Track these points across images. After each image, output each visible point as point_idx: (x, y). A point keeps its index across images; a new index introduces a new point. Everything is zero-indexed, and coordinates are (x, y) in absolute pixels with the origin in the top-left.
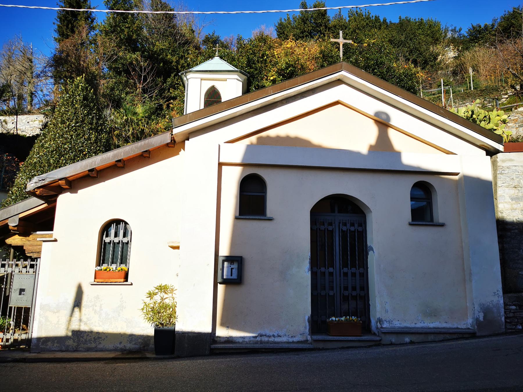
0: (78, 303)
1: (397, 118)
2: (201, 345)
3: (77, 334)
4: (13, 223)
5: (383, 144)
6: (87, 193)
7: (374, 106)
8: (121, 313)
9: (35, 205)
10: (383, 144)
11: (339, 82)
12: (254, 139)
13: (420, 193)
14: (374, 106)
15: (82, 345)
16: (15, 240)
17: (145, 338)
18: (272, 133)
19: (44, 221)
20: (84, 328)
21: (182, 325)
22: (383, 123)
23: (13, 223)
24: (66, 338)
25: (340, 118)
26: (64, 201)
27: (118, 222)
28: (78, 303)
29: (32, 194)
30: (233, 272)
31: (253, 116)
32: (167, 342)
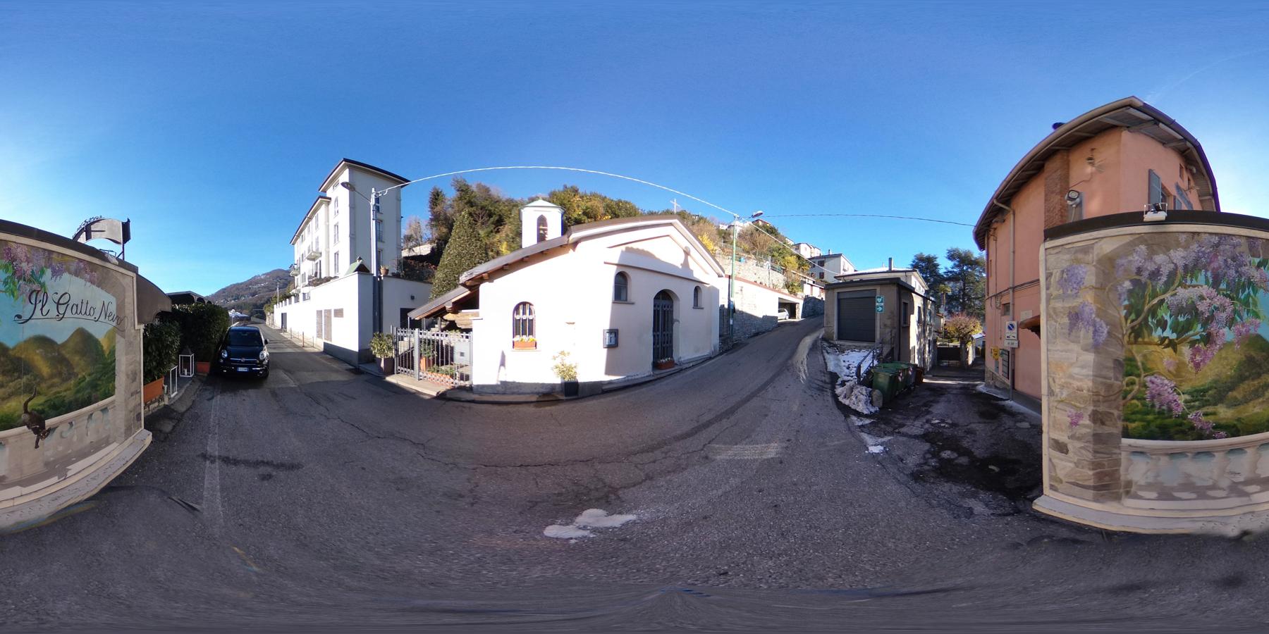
0: (503, 364)
1: (693, 252)
2: (596, 390)
3: (504, 384)
4: (448, 307)
5: (686, 264)
6: (500, 282)
7: (685, 244)
8: (535, 368)
9: (462, 293)
10: (686, 264)
11: (671, 224)
12: (623, 248)
13: (83, 368)
14: (685, 244)
15: (507, 397)
16: (449, 317)
17: (553, 386)
18: (634, 246)
19: (471, 302)
20: (510, 379)
21: (583, 377)
22: (687, 253)
23: (448, 307)
24: (496, 386)
25: (668, 246)
26: (484, 288)
27: (524, 304)
28: (503, 364)
29: (464, 285)
30: (614, 339)
31: (519, 385)
32: (572, 390)
